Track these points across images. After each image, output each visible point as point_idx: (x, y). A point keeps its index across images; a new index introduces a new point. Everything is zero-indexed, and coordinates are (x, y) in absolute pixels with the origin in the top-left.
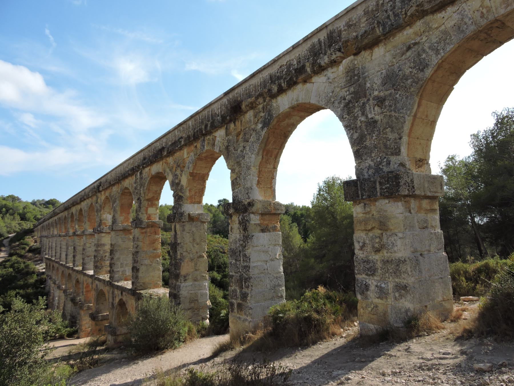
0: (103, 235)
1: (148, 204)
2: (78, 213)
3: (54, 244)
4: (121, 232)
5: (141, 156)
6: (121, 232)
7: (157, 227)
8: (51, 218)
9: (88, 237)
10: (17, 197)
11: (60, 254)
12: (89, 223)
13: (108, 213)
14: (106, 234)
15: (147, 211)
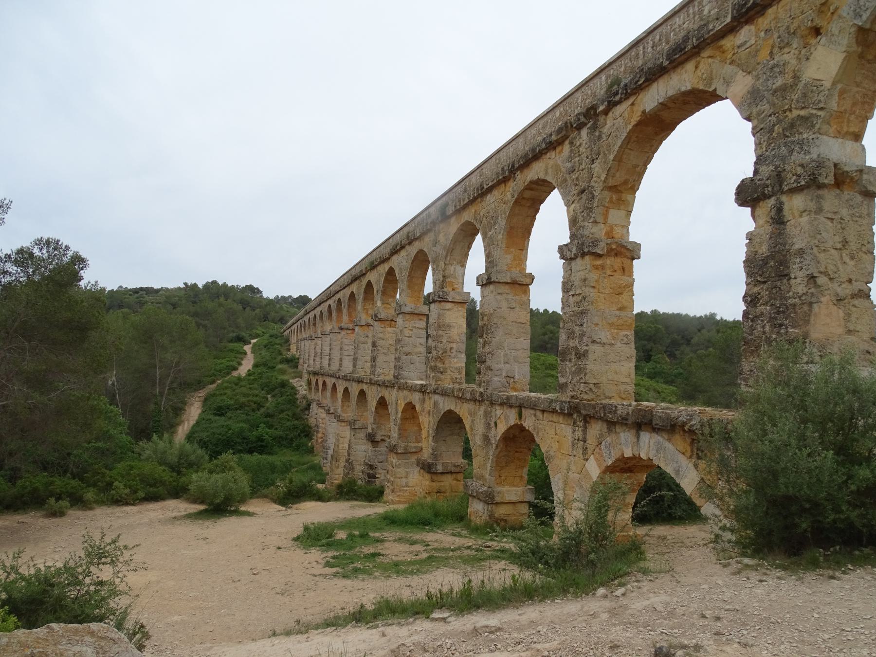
0: (448, 306)
1: (611, 201)
2: (383, 280)
3: (327, 349)
4: (507, 287)
5: (367, 261)
6: (505, 289)
7: (626, 256)
8: (320, 305)
9: (408, 317)
10: (258, 289)
11: (341, 360)
12: (409, 291)
13: (458, 263)
14: (453, 304)
15: (606, 216)
